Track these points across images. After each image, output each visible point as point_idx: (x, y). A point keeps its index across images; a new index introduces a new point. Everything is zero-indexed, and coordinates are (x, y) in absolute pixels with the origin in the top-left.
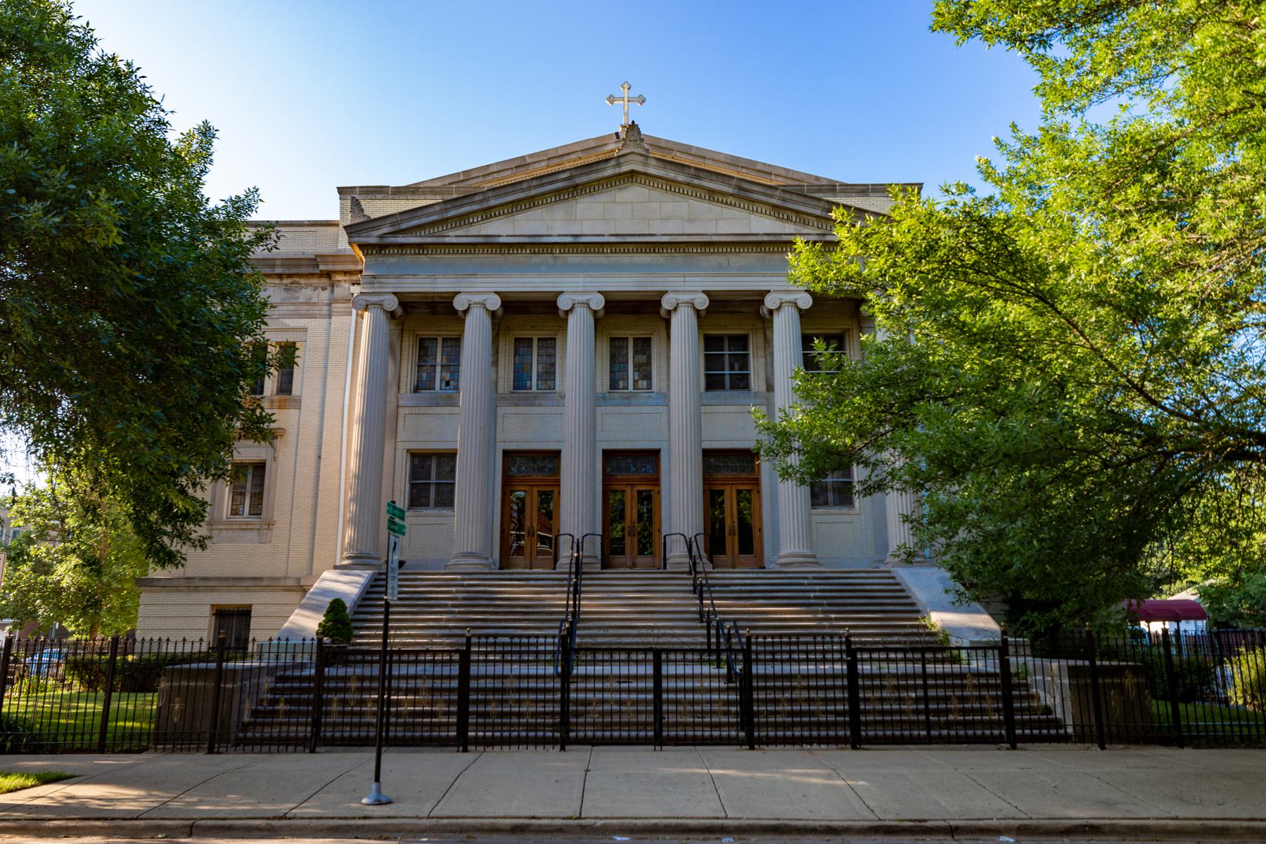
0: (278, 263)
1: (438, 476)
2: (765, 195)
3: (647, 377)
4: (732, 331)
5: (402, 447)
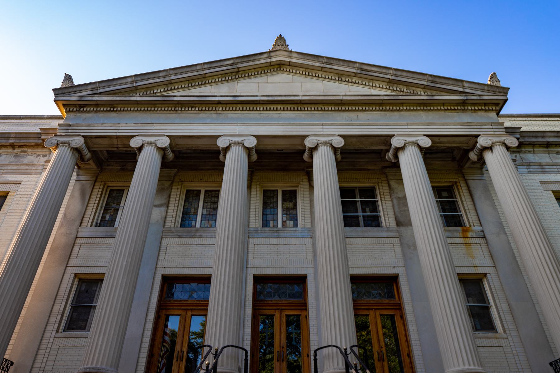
0: (12, 136)
2: (382, 73)
3: (295, 219)
4: (367, 169)
5: (71, 271)
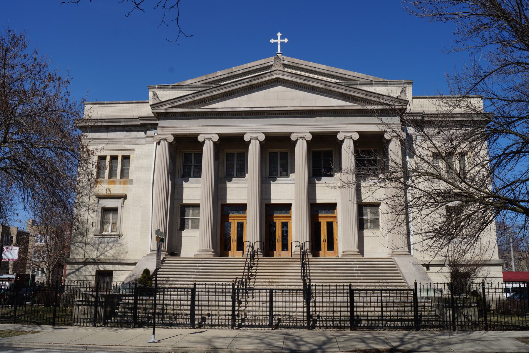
1: (193, 215)
